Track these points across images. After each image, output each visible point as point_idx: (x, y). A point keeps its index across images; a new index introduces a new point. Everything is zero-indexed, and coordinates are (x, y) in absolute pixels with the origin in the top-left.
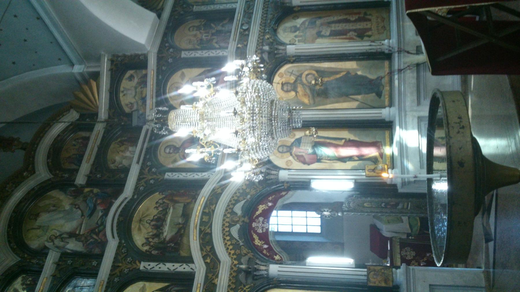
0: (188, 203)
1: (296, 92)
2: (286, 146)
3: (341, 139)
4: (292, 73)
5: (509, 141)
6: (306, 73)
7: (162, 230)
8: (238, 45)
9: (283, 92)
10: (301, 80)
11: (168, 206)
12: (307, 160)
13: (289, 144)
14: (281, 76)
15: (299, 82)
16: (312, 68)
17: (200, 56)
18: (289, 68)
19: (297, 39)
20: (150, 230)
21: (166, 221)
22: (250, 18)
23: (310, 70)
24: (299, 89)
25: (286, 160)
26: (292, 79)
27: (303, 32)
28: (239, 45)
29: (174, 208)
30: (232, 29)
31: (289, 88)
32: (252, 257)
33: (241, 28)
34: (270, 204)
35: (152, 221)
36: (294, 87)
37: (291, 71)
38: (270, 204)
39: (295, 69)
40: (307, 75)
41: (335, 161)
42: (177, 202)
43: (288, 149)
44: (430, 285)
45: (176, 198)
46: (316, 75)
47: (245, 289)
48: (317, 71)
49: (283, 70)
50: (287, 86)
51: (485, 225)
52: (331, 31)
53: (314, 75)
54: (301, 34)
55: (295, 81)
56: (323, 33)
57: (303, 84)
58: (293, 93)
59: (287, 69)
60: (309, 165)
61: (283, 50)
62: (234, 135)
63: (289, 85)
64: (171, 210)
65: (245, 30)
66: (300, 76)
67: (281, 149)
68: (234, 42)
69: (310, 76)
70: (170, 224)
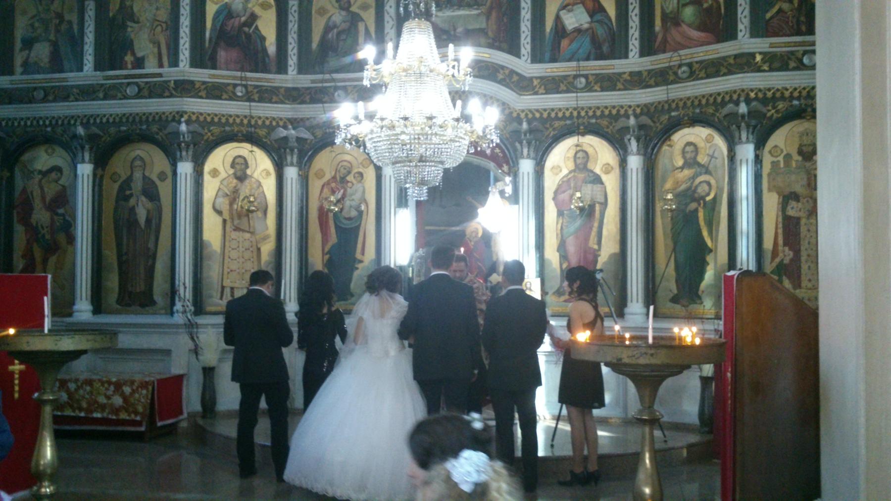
0: (486, 34)
1: (682, 168)
2: (587, 161)
3: (599, 243)
4: (712, 157)
6: (713, 182)
7: (446, 7)
8: (760, 53)
9: (683, 145)
10: (701, 174)
11: (482, 5)
13: (590, 166)
14: (709, 139)
15: (699, 170)
16: (720, 190)
17: (188, 19)
18: (722, 153)
19: (781, 158)
21: (459, 9)
23: (717, 187)
24: (687, 172)
25: (562, 165)
26: (702, 159)
27: (798, 168)
28: (758, 58)
29: (478, 15)
30: (221, 69)
31: (688, 156)
36: (691, 163)
37: (716, 155)
39: (719, 162)
40: (709, 184)
42: (488, 16)
43: (581, 166)
45: (494, 14)
46: (708, 199)
47: (773, 111)
48: (715, 199)
50: (583, 158)
52: (798, 219)
53: (708, 194)
54: (794, 164)
55: (699, 165)
56: (793, 203)
57: (693, 178)
58: (680, 162)
60: (554, 199)
63: (694, 154)
64: (475, 12)
65: (676, 74)
66: (708, 172)
67: (580, 155)
68: (768, 45)
69: (706, 188)
70: (453, 17)
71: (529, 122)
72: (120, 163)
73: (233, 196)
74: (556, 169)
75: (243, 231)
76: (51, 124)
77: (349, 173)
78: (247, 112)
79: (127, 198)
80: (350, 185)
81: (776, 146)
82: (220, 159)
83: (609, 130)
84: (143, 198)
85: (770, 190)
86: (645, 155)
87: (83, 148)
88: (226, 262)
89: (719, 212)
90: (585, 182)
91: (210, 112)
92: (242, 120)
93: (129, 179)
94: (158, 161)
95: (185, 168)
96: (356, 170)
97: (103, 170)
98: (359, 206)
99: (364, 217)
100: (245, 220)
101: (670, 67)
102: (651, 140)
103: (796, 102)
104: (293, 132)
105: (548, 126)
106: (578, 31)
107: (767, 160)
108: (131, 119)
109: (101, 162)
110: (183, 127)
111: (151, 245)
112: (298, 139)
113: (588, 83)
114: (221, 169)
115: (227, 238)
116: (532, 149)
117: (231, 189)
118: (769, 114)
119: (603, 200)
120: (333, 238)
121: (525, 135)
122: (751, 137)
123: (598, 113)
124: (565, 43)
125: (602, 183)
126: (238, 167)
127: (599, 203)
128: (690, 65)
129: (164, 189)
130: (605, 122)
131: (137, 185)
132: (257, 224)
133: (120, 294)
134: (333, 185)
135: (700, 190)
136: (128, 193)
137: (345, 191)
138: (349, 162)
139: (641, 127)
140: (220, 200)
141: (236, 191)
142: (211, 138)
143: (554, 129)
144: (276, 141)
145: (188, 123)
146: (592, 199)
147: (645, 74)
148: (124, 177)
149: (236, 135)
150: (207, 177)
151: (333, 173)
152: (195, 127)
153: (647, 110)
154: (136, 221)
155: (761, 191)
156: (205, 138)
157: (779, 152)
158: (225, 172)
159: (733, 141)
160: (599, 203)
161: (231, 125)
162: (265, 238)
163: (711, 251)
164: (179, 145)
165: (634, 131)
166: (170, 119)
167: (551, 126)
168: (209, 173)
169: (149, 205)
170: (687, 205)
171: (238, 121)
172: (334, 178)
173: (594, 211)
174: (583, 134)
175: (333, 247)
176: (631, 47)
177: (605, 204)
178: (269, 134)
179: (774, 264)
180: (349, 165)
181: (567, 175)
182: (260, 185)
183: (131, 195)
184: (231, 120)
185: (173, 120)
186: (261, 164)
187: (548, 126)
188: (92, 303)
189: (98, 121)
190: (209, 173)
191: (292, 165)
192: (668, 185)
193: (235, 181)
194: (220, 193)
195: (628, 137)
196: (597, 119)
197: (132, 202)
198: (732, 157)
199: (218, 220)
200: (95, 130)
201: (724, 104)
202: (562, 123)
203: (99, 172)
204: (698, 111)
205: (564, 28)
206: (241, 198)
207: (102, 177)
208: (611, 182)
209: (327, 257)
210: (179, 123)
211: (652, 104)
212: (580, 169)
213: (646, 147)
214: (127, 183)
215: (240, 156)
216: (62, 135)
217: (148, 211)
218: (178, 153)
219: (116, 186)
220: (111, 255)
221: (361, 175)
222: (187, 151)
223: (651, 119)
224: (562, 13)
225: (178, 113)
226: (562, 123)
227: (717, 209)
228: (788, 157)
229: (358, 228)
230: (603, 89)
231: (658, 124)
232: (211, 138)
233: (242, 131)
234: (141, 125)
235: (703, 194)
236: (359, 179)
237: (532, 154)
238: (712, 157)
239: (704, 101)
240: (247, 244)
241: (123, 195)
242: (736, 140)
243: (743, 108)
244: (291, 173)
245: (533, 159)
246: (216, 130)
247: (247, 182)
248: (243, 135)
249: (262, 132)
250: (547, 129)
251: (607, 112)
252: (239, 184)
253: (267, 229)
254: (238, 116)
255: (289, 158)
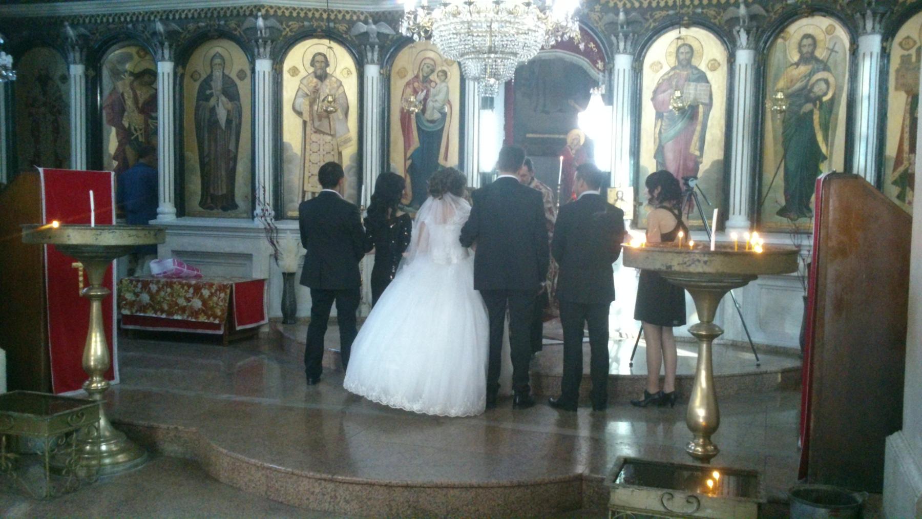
1: (797, 64)
3: (701, 149)
4: (832, 50)
5: (626, 441)
6: (831, 80)
10: (818, 71)
12: (661, 97)
13: (694, 62)
14: (830, 31)
16: (839, 89)
19: (913, 52)
24: (803, 69)
26: (820, 54)
32: (284, 33)
34: (582, 46)
36: (808, 58)
37: (836, 49)
38: (582, 46)
40: (827, 82)
41: (658, 141)
44: (284, 274)
46: (825, 99)
48: (832, 100)
51: (891, 150)
53: (825, 94)
55: (817, 60)
57: (811, 74)
58: (796, 58)
59: (841, 40)
60: (653, 99)
66: (826, 68)
69: (823, 86)
71: (627, 12)
72: (199, 61)
73: (314, 96)
74: (657, 65)
75: (324, 133)
76: (131, 21)
77: (433, 71)
79: (208, 98)
80: (433, 84)
81: (908, 37)
82: (299, 56)
83: (717, 21)
84: (223, 98)
85: (896, 89)
86: (756, 49)
87: (162, 44)
88: (307, 165)
89: (837, 115)
90: (688, 80)
91: (288, 6)
92: (321, 14)
93: (210, 77)
94: (235, 57)
95: (263, 66)
96: (440, 69)
97: (184, 67)
98: (442, 108)
99: (448, 119)
100: (325, 122)
102: (763, 32)
104: (374, 27)
105: (648, 17)
108: (209, 15)
109: (181, 59)
110: (260, 22)
111: (232, 147)
112: (379, 34)
114: (301, 68)
115: (308, 140)
116: (629, 43)
117: (311, 89)
119: (707, 101)
120: (416, 143)
121: (622, 27)
122: (877, 26)
125: (708, 82)
126: (317, 65)
127: (703, 104)
129: (243, 87)
130: (712, 12)
131: (217, 85)
132: (338, 127)
133: (202, 195)
134: (416, 85)
135: (816, 89)
136: (208, 92)
137: (428, 91)
138: (433, 60)
139: (753, 17)
140: (300, 101)
141: (316, 91)
142: (290, 34)
143: (655, 21)
144: (356, 36)
145: (265, 17)
146: (695, 99)
148: (204, 76)
149: (315, 31)
150: (286, 76)
151: (416, 73)
152: (272, 22)
154: (217, 122)
155: (887, 89)
156: (284, 33)
157: (911, 43)
158: (305, 70)
159: (857, 32)
160: (703, 104)
161: (310, 20)
162: (349, 140)
163: (825, 158)
164: (257, 41)
165: (744, 22)
166: (247, 13)
167: (652, 16)
168: (289, 71)
169: (230, 105)
170: (801, 106)
171: (317, 15)
172: (417, 77)
173: (697, 113)
174: (687, 26)
175: (416, 150)
177: (709, 106)
178: (349, 29)
179: (897, 174)
180: (432, 63)
181: (668, 73)
182: (341, 84)
183: (211, 95)
184: (310, 15)
185: (251, 14)
186: (341, 61)
187: (648, 17)
188: (176, 206)
189: (177, 17)
190: (289, 71)
191: (373, 62)
192: (781, 84)
193: (315, 80)
194: (300, 93)
195: (737, 28)
196: (703, 8)
197: (213, 102)
198: (854, 51)
199: (298, 121)
200: (82, 30)
202: (664, 13)
203: (180, 70)
206: (322, 98)
207: (182, 75)
208: (718, 80)
209: (409, 162)
210: (256, 17)
212: (683, 66)
213: (757, 42)
214: (207, 82)
215: (320, 54)
216: (143, 32)
217: (228, 111)
218: (256, 50)
219: (197, 85)
220: (193, 156)
221: (445, 73)
222: (265, 48)
223: (764, 8)
225: (255, 7)
226: (664, 13)
227: (834, 111)
229: (442, 130)
231: (772, 14)
232: (290, 34)
233: (321, 27)
234: (219, 21)
235: (820, 93)
236: (443, 78)
237: (629, 48)
238: (832, 50)
240: (328, 148)
241: (204, 95)
242: (860, 31)
244: (372, 71)
245: (630, 54)
246: (295, 25)
247: (327, 82)
248: (322, 31)
249: (342, 27)
250: (647, 20)
252: (319, 83)
253: (348, 130)
254: (317, 10)
255: (369, 55)
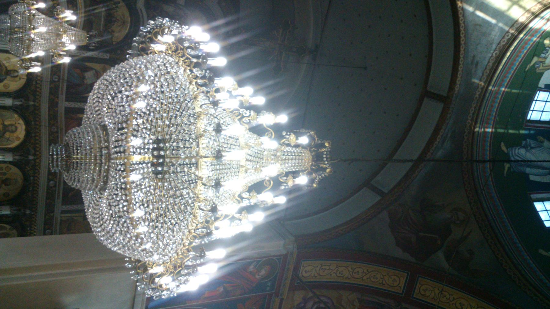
1: (3, 124)
14: (18, 138)
19: (4, 171)
20: (115, 14)
22: (48, 193)
26: (7, 135)
33: (56, 182)
35: (115, 21)
49: (17, 143)
59: (12, 144)
61: (16, 155)
62: (233, 224)
64: (102, 28)
65: (52, 180)
78: (43, 124)
81: (11, 169)
101: (57, 122)
103: (32, 178)
106: (84, 78)
107: (4, 166)
113: (55, 82)
118: (27, 167)
123: (38, 86)
124: (78, 71)
128: (57, 132)
139: (28, 107)
147: (56, 109)
153: (37, 109)
176: (71, 103)
195: (23, 101)
201: (36, 151)
204: (33, 135)
205: (86, 71)
211: (40, 112)
224: (94, 71)
228: (5, 174)
230: (51, 89)
239: (37, 138)
243: (31, 157)
251: (38, 90)
255: (17, 157)
